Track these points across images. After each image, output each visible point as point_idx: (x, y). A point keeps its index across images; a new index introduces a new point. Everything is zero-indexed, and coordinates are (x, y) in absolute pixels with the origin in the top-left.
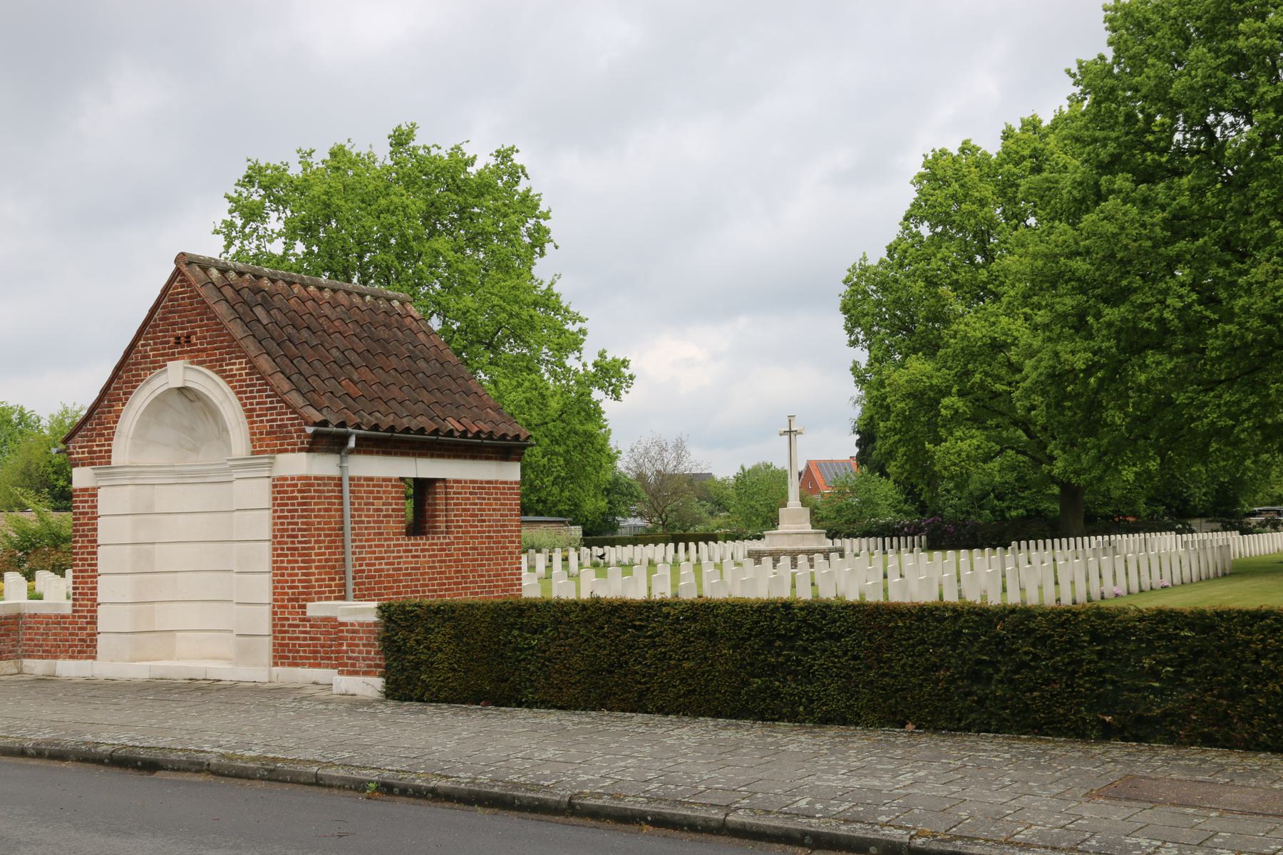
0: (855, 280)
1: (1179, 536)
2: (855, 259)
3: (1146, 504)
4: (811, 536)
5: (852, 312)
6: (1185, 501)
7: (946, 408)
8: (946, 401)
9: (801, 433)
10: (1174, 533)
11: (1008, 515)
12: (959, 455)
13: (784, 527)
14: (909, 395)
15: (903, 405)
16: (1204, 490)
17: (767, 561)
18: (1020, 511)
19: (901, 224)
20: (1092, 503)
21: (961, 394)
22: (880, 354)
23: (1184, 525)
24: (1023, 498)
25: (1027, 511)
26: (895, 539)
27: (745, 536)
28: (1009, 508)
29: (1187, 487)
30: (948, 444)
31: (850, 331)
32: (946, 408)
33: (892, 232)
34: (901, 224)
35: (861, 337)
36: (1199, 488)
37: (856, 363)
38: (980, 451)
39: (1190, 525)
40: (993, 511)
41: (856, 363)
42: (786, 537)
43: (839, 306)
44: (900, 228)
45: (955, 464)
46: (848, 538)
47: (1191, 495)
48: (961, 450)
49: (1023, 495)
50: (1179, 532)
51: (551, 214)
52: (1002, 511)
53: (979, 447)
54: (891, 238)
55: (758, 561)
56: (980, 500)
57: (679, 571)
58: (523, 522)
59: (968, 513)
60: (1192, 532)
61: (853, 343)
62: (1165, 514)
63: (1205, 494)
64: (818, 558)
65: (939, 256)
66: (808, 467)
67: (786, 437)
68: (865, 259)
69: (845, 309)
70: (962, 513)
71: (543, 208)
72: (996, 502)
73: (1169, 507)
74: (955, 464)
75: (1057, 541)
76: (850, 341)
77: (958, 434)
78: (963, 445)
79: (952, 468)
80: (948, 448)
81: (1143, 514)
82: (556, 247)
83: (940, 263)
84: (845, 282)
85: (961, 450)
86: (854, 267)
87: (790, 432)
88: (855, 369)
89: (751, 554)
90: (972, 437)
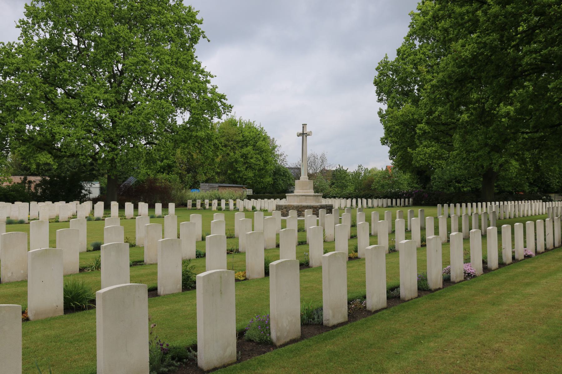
0: (382, 68)
1: (544, 203)
2: (382, 58)
3: (529, 186)
4: (312, 198)
5: (380, 84)
6: (548, 186)
7: (420, 129)
8: (419, 126)
9: (309, 135)
10: (541, 201)
11: (462, 190)
12: (425, 155)
13: (298, 191)
14: (402, 123)
15: (397, 127)
16: (557, 180)
17: (293, 213)
18: (468, 188)
19: (405, 38)
20: (503, 185)
21: (427, 123)
22: (392, 104)
23: (547, 197)
24: (470, 182)
25: (472, 188)
26: (398, 200)
27: (328, 196)
28: (463, 187)
29: (549, 179)
30: (420, 149)
31: (379, 94)
32: (420, 129)
33: (399, 42)
34: (405, 38)
35: (384, 98)
36: (555, 179)
37: (381, 109)
38: (437, 154)
39: (550, 197)
40: (455, 188)
41: (381, 109)
42: (296, 197)
43: (373, 81)
44: (404, 40)
45: (423, 160)
46: (376, 199)
47: (551, 183)
48: (426, 153)
49: (470, 181)
50: (544, 201)
51: (203, 22)
52: (459, 188)
53: (436, 151)
54: (399, 46)
55: (285, 214)
56: (449, 183)
57: (104, 226)
58: (219, 186)
59: (443, 188)
60: (551, 201)
61: (380, 100)
62: (538, 191)
63: (558, 182)
64: (308, 214)
65: (421, 52)
66: (386, 169)
67: (301, 137)
68: (386, 57)
69: (376, 83)
70: (441, 188)
71: (198, 17)
72: (457, 184)
73: (540, 188)
74: (423, 160)
75: (474, 204)
76: (379, 99)
77: (425, 143)
78: (428, 150)
79: (421, 162)
80: (420, 151)
81: (527, 191)
82: (209, 41)
83: (421, 55)
84: (377, 69)
85: (426, 153)
86: (381, 62)
87: (303, 134)
88: (380, 113)
89: (279, 208)
90: (433, 146)
